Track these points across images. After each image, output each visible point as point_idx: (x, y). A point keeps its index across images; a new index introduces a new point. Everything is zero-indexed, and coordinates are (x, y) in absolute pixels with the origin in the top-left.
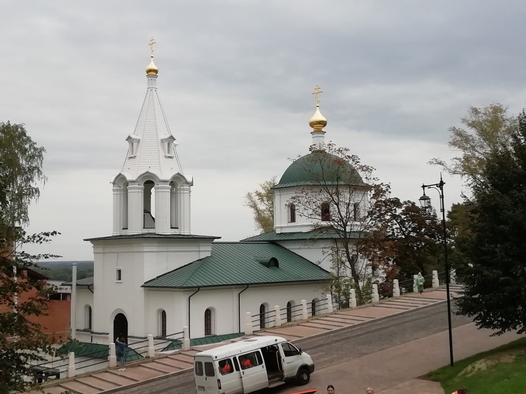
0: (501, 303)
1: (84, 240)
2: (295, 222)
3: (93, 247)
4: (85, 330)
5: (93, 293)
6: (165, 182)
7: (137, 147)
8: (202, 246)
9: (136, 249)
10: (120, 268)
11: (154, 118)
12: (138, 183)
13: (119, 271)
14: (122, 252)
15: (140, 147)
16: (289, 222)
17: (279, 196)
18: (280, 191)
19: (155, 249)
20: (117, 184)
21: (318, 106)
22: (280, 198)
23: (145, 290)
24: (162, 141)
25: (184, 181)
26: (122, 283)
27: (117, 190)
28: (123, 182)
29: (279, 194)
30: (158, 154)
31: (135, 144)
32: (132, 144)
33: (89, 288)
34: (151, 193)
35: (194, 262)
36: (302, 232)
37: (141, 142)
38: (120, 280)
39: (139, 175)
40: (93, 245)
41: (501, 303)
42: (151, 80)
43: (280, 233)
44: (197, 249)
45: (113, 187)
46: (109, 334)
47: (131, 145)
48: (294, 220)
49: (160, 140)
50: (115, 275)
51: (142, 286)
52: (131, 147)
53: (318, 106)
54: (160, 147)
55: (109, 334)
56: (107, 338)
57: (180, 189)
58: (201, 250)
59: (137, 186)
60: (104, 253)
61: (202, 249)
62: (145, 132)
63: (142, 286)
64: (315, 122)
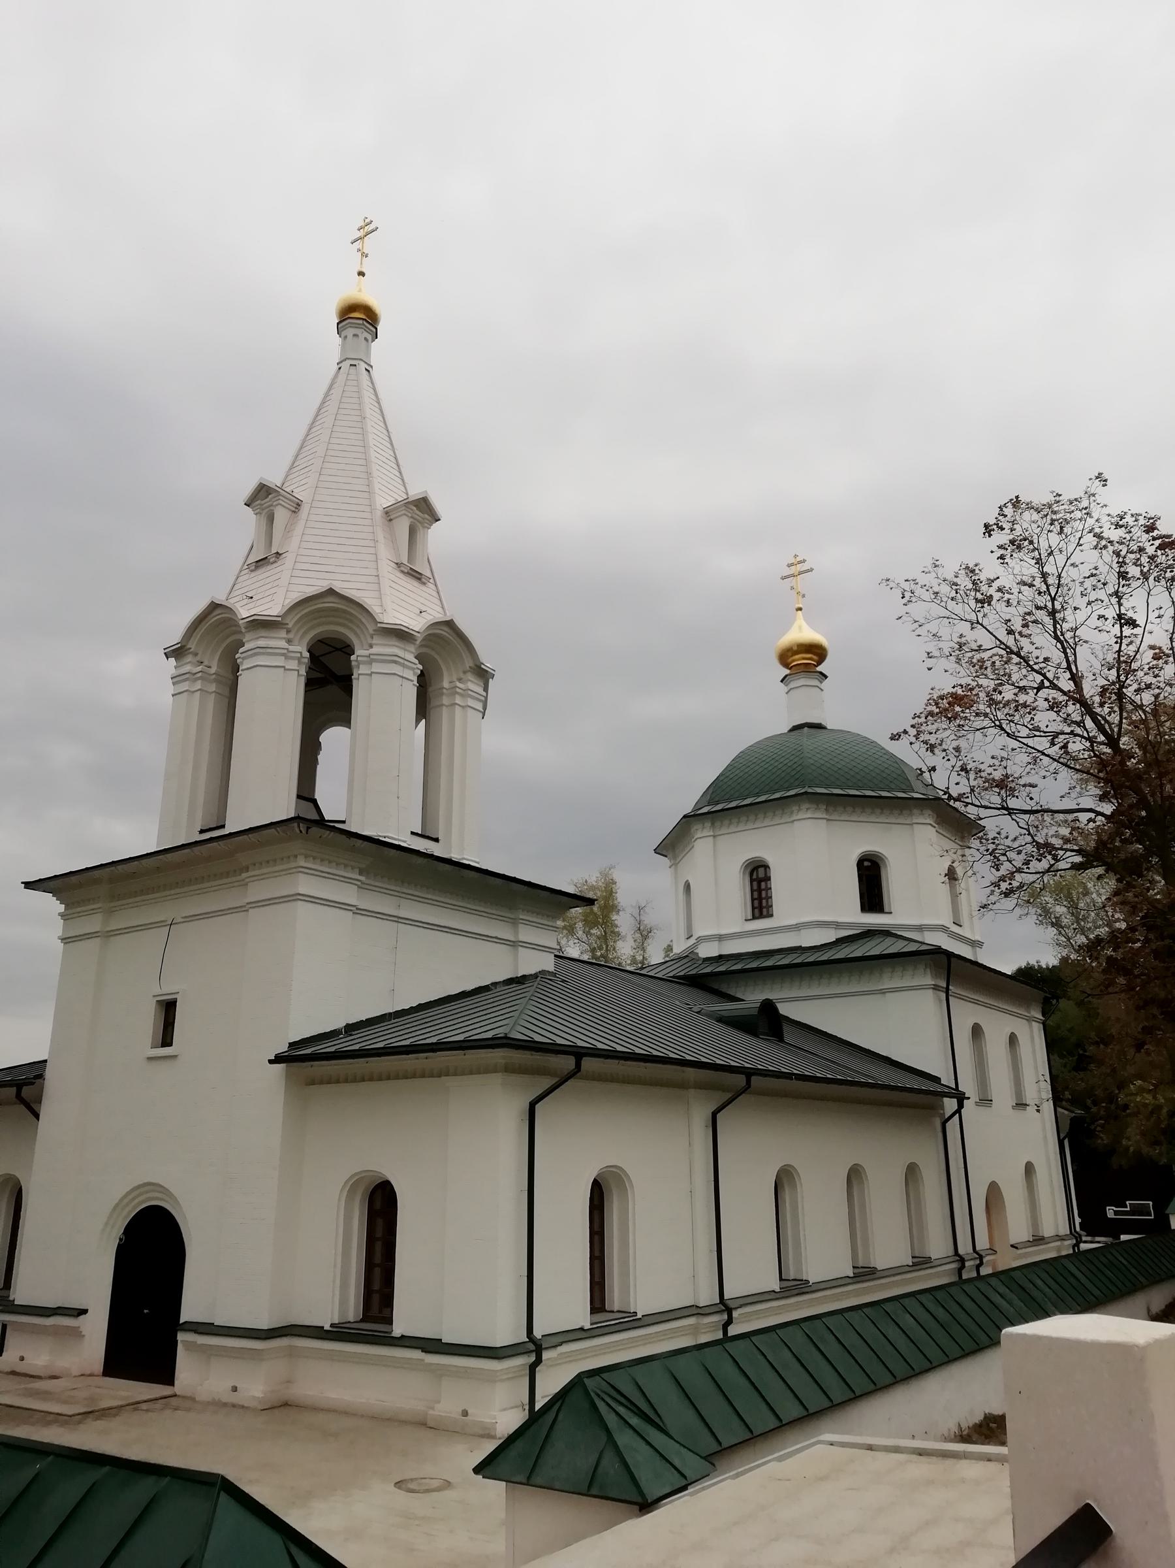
0: (146, 1311)
1: (28, 885)
2: (772, 915)
3: (62, 915)
4: (339, 1333)
5: (37, 1116)
6: (400, 634)
7: (288, 529)
8: (529, 923)
9: (258, 890)
10: (168, 989)
11: (361, 443)
12: (283, 634)
13: (169, 1008)
14: (189, 919)
15: (301, 523)
16: (746, 920)
17: (712, 837)
18: (713, 824)
19: (349, 894)
20: (196, 654)
21: (800, 609)
22: (714, 841)
23: (288, 1076)
24: (389, 514)
25: (469, 663)
26: (174, 1057)
27: (191, 677)
28: (224, 645)
29: (712, 834)
30: (372, 550)
31: (281, 515)
32: (271, 519)
33: (20, 1099)
34: (320, 743)
35: (495, 984)
36: (800, 948)
37: (305, 509)
38: (170, 1044)
39: (295, 596)
40: (62, 908)
41: (146, 1311)
42: (355, 335)
43: (716, 954)
44: (504, 931)
45: (176, 667)
46: (84, 1312)
47: (264, 522)
48: (761, 908)
49: (379, 513)
50: (148, 1021)
51: (278, 1059)
52: (264, 528)
53: (800, 609)
54: (380, 536)
55: (84, 1312)
56: (76, 1334)
57: (453, 691)
58: (521, 938)
59: (283, 644)
60: (108, 935)
61: (526, 934)
62: (334, 435)
63: (278, 1059)
64: (795, 648)
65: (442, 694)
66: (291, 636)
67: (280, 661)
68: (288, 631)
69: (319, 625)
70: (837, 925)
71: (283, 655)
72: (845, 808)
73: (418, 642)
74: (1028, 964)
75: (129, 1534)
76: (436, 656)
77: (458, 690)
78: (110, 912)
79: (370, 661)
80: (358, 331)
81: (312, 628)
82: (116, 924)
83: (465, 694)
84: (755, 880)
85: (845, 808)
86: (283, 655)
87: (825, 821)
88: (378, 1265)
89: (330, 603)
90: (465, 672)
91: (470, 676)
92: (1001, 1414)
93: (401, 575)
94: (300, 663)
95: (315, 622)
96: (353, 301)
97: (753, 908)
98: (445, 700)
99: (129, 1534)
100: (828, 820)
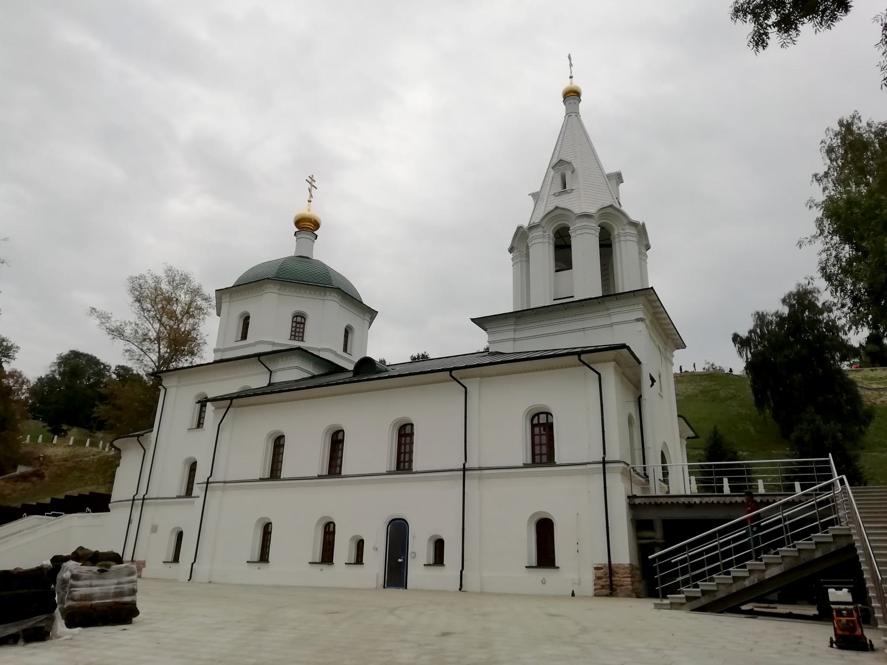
12: (541, 229)
25: (625, 221)
65: (615, 238)
66: (544, 229)
67: (541, 240)
68: (543, 228)
69: (556, 222)
70: (274, 344)
71: (541, 237)
72: (290, 289)
73: (596, 218)
74: (761, 318)
75: (124, 548)
76: (611, 223)
77: (621, 234)
78: (515, 330)
79: (575, 231)
80: (570, 101)
81: (552, 226)
82: (519, 335)
83: (626, 235)
84: (294, 322)
85: (290, 289)
86: (541, 237)
87: (278, 294)
88: (544, 444)
89: (557, 212)
90: (624, 226)
91: (627, 227)
92: (269, 560)
93: (559, 197)
94: (549, 239)
95: (552, 223)
96: (578, 90)
97: (291, 335)
98: (617, 240)
99: (124, 548)
100: (279, 294)
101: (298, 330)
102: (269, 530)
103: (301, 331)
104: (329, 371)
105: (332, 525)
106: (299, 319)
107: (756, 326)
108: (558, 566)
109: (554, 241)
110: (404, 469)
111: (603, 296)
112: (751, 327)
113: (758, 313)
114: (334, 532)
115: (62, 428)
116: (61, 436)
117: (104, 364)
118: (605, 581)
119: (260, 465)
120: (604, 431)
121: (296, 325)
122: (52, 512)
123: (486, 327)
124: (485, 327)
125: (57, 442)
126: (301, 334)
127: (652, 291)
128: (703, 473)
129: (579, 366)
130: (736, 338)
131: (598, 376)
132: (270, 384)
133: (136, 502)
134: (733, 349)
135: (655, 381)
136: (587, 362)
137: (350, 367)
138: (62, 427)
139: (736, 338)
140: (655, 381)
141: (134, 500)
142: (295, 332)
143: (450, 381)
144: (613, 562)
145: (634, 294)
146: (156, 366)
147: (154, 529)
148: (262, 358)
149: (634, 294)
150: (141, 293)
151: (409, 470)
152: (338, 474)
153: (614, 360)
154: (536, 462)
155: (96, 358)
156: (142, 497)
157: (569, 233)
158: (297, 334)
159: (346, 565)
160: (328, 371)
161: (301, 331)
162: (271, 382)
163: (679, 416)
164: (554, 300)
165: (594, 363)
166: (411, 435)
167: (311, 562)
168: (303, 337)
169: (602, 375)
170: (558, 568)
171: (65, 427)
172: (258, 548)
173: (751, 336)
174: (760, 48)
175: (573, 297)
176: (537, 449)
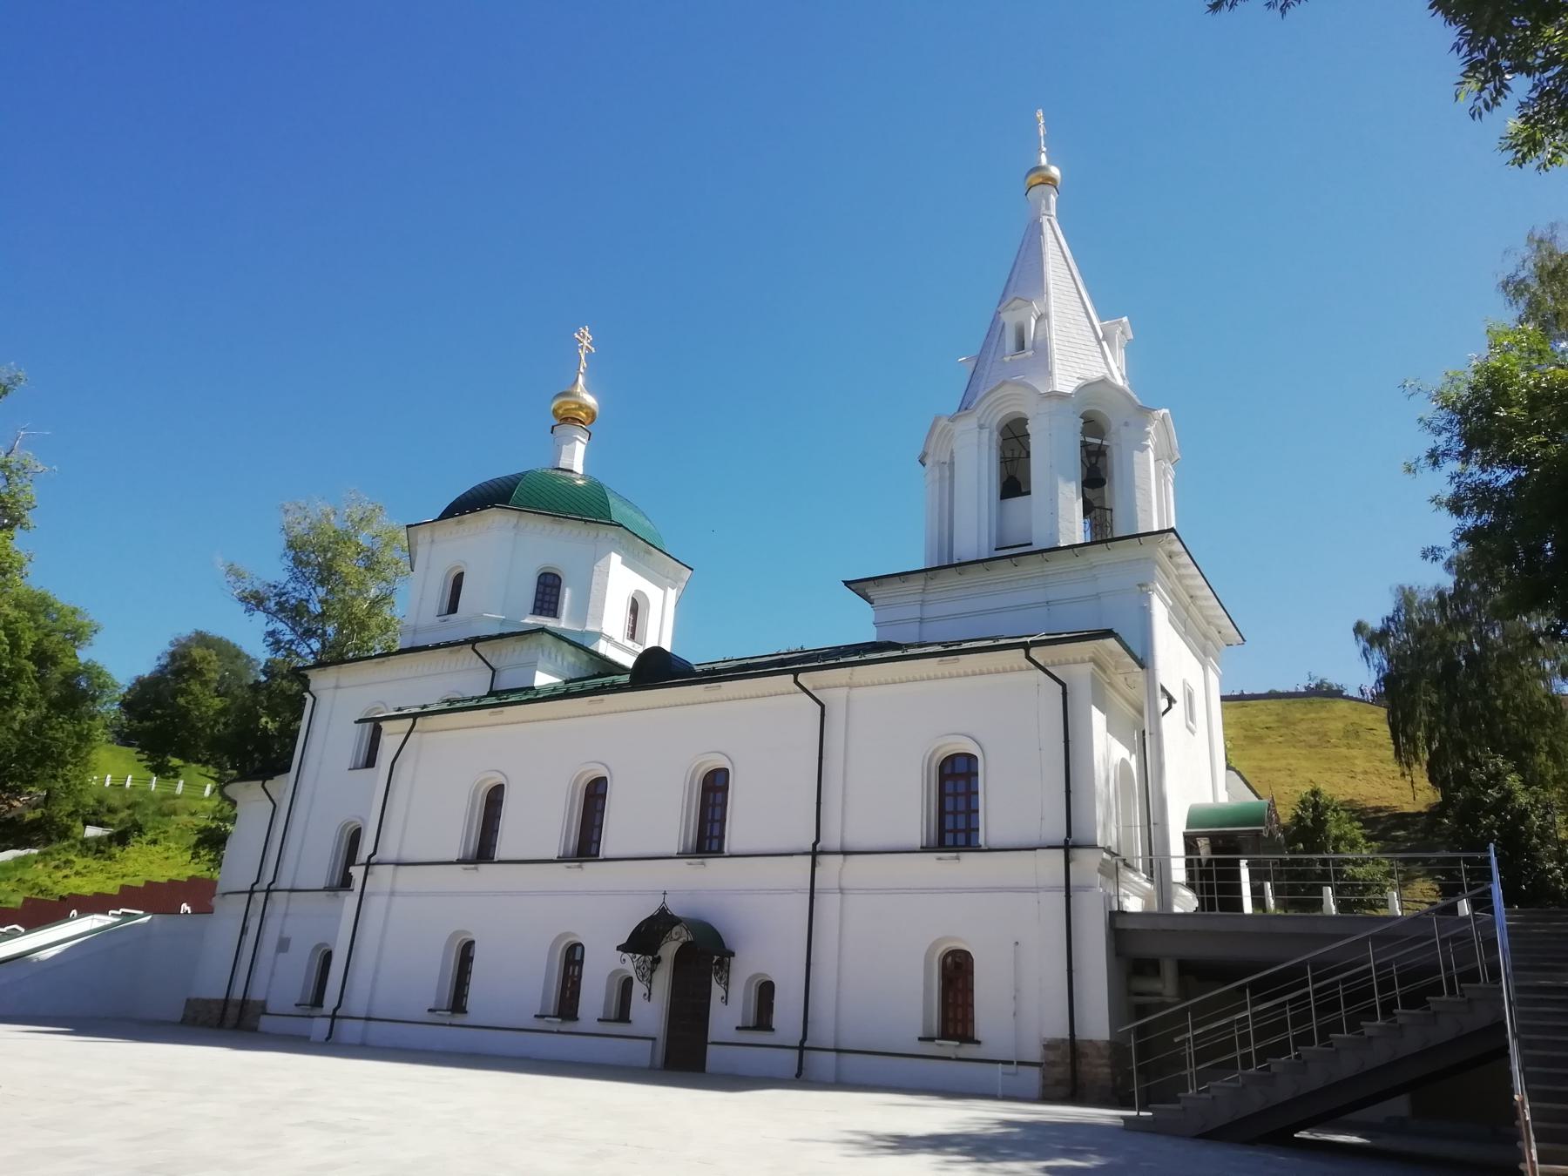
101: (547, 598)
102: (471, 955)
103: (547, 604)
104: (599, 673)
105: (579, 948)
106: (549, 580)
107: (1398, 610)
108: (979, 1039)
109: (1000, 444)
110: (710, 851)
111: (1092, 543)
112: (1390, 613)
113: (1402, 588)
114: (581, 963)
115: (170, 764)
116: (168, 778)
117: (248, 657)
118: (1061, 1071)
119: (456, 836)
120: (1070, 791)
121: (544, 590)
122: (122, 910)
123: (872, 597)
124: (869, 597)
125: (183, 791)
126: (552, 606)
127: (1172, 535)
128: (1292, 875)
129: (1028, 669)
130: (1359, 629)
131: (1061, 687)
132: (491, 693)
133: (256, 895)
134: (1354, 648)
135: (1175, 702)
136: (1041, 663)
137: (629, 661)
138: (169, 761)
139: (1359, 629)
140: (1175, 702)
141: (252, 892)
142: (542, 601)
143: (796, 693)
144: (1077, 1038)
145: (1140, 541)
146: (1361, 828)
147: (283, 945)
148: (478, 646)
149: (1140, 541)
150: (283, 529)
151: (718, 852)
152: (592, 856)
153: (1093, 660)
154: (947, 844)
155: (228, 642)
156: (266, 888)
157: (1026, 430)
158: (546, 606)
159: (536, 1019)
160: (596, 673)
161: (547, 604)
162: (494, 688)
163: (1229, 767)
164: (996, 549)
165: (1053, 665)
166: (725, 789)
167: (740, 1025)
168: (556, 613)
169: (1171, 710)
170: (978, 1042)
171: (175, 762)
172: (315, 970)
173: (1389, 627)
174: (1510, 154)
175: (1030, 544)
176: (949, 820)
